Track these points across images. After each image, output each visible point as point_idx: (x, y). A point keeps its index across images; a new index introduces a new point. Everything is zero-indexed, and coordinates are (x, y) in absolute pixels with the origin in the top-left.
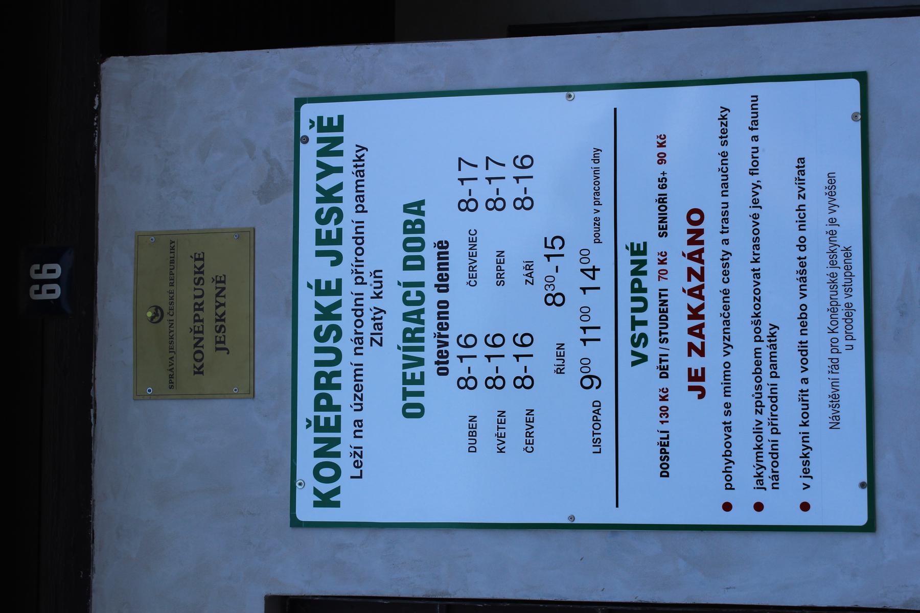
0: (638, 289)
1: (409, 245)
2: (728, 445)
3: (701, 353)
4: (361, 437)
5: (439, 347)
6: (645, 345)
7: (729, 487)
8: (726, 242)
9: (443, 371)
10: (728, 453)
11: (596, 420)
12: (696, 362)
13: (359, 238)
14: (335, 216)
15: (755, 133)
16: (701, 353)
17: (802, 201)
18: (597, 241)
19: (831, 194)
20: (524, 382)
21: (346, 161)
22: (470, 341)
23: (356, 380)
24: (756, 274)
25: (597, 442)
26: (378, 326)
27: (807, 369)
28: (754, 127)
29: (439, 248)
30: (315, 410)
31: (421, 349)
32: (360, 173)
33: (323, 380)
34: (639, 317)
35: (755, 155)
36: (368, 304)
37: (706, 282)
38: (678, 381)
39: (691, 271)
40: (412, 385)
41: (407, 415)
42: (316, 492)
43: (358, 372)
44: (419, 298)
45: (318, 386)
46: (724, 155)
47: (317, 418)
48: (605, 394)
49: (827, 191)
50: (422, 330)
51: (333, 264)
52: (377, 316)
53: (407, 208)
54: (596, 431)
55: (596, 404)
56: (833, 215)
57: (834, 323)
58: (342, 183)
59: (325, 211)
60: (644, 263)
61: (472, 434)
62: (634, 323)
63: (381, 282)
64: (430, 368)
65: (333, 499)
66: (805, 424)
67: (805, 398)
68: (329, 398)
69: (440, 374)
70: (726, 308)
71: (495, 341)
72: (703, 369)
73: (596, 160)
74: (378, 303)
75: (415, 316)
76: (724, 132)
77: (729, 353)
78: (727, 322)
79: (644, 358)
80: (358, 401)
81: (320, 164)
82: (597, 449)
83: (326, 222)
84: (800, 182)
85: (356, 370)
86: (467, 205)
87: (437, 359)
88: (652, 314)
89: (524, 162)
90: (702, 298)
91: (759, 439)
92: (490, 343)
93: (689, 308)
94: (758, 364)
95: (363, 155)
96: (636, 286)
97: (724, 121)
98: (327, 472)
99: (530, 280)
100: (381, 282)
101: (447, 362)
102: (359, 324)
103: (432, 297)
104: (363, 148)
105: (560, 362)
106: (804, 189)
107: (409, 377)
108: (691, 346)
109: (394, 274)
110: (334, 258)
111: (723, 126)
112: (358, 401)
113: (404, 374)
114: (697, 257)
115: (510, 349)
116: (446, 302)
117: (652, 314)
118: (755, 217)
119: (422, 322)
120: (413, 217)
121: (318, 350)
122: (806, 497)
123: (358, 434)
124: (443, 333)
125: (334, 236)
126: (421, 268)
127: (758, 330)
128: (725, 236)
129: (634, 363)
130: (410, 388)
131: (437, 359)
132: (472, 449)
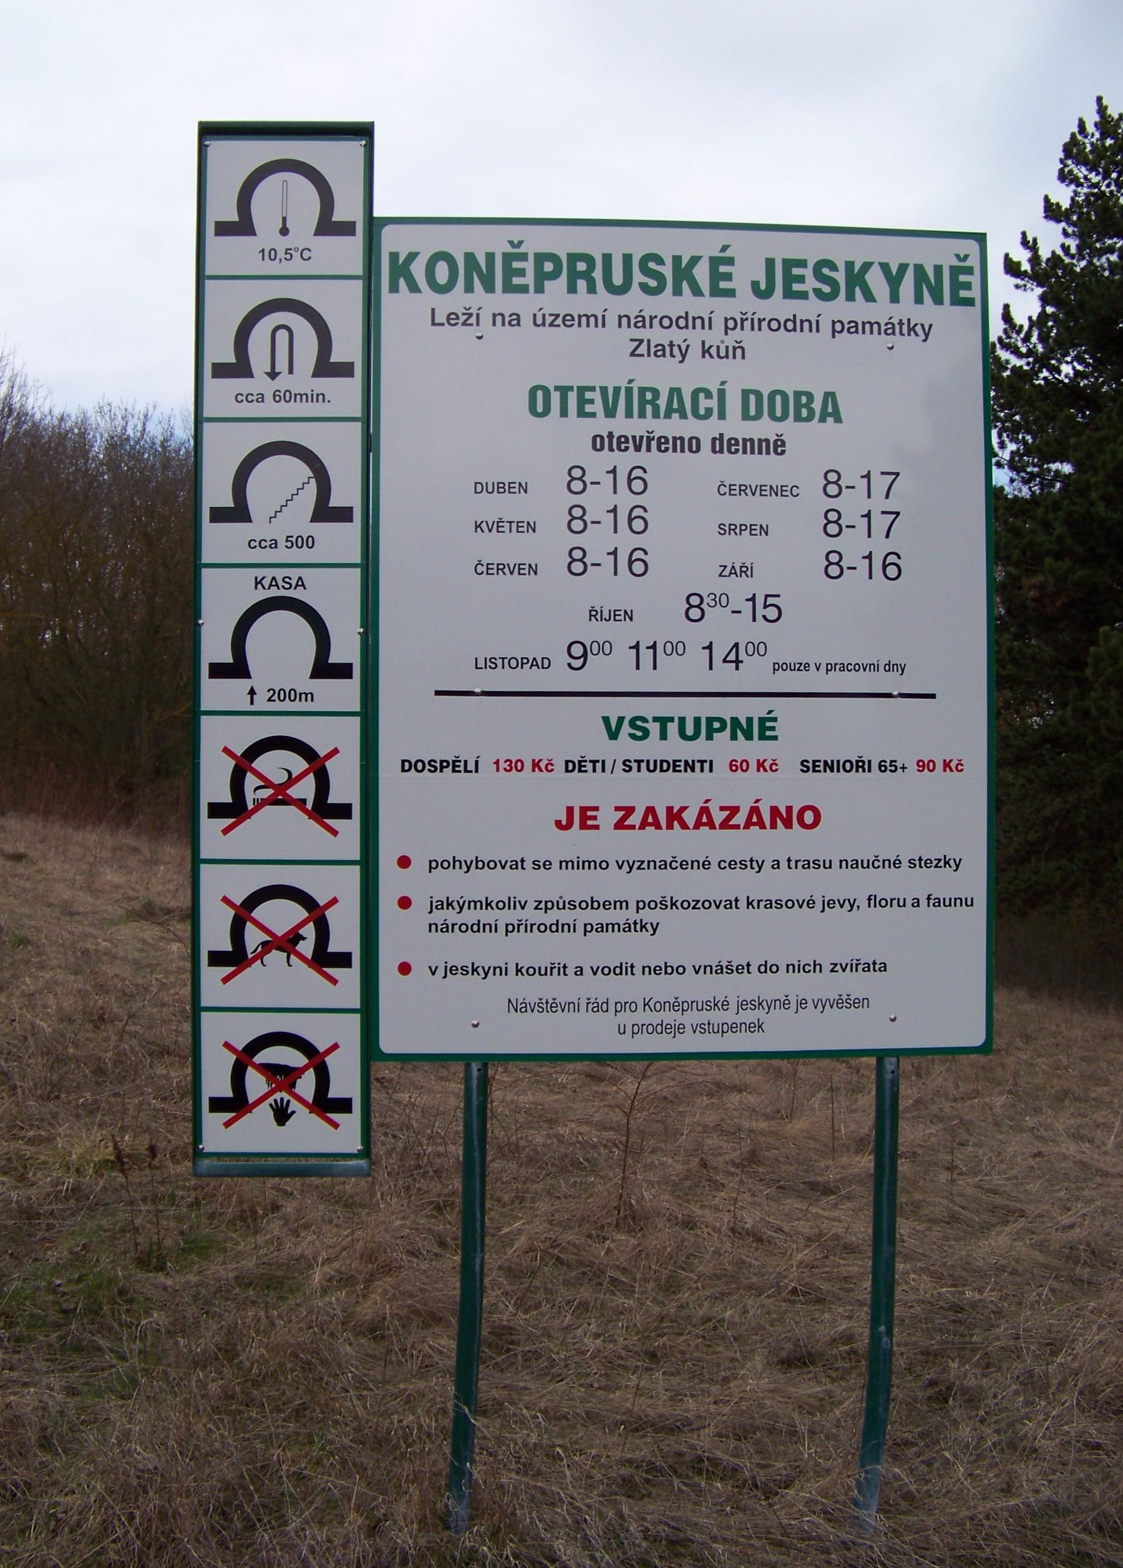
0: (712, 727)
1: (778, 398)
2: (492, 865)
3: (620, 825)
4: (494, 324)
5: (634, 437)
6: (633, 736)
7: (433, 865)
8: (776, 865)
9: (598, 443)
10: (480, 865)
12: (607, 817)
13: (793, 325)
14: (826, 289)
15: (923, 902)
16: (620, 825)
17: (827, 967)
18: (777, 667)
19: (839, 1003)
20: (578, 562)
21: (907, 309)
22: (638, 525)
23: (580, 317)
24: (732, 904)
26: (661, 351)
27: (595, 974)
28: (932, 902)
29: (776, 441)
30: (536, 254)
31: (629, 414)
32: (890, 329)
33: (581, 266)
34: (673, 728)
35: (895, 902)
36: (694, 337)
37: (718, 831)
38: (581, 790)
39: (734, 810)
40: (577, 399)
41: (533, 391)
42: (412, 256)
43: (592, 320)
44: (702, 412)
45: (573, 258)
46: (896, 863)
47: (524, 257)
49: (844, 997)
50: (656, 415)
51: (755, 285)
52: (676, 350)
53: (830, 396)
56: (810, 1004)
57: (658, 1006)
58: (875, 301)
59: (832, 274)
60: (748, 736)
62: (663, 721)
63: (727, 356)
64: (602, 425)
65: (402, 281)
66: (518, 971)
67: (555, 971)
68: (555, 275)
69: (594, 438)
70: (683, 865)
71: (639, 522)
72: (597, 827)
73: (890, 667)
74: (695, 351)
75: (676, 406)
76: (928, 863)
77: (620, 868)
78: (664, 865)
79: (613, 735)
80: (549, 320)
81: (903, 268)
83: (818, 276)
84: (854, 966)
85: (596, 317)
86: (832, 482)
87: (616, 435)
88: (675, 748)
89: (892, 566)
90: (697, 826)
91: (501, 905)
92: (636, 555)
93: (683, 809)
94: (606, 905)
95: (917, 335)
96: (716, 725)
97: (942, 864)
98: (442, 273)
99: (727, 572)
100: (727, 356)
101: (611, 449)
102: (666, 322)
103: (706, 430)
104: (927, 335)
105: (606, 615)
106: (844, 970)
107: (588, 395)
108: (629, 811)
109: (737, 377)
110: (763, 287)
111: (935, 863)
112: (549, 320)
113: (593, 389)
114: (755, 818)
115: (626, 542)
116: (698, 450)
117: (675, 748)
118: (811, 903)
119: (668, 416)
120: (817, 406)
121: (627, 259)
122: (419, 970)
123: (499, 319)
124: (654, 444)
125: (796, 287)
126: (746, 416)
127: (653, 905)
128: (784, 864)
129: (606, 720)
130: (572, 397)
131: (616, 435)
132: (480, 488)
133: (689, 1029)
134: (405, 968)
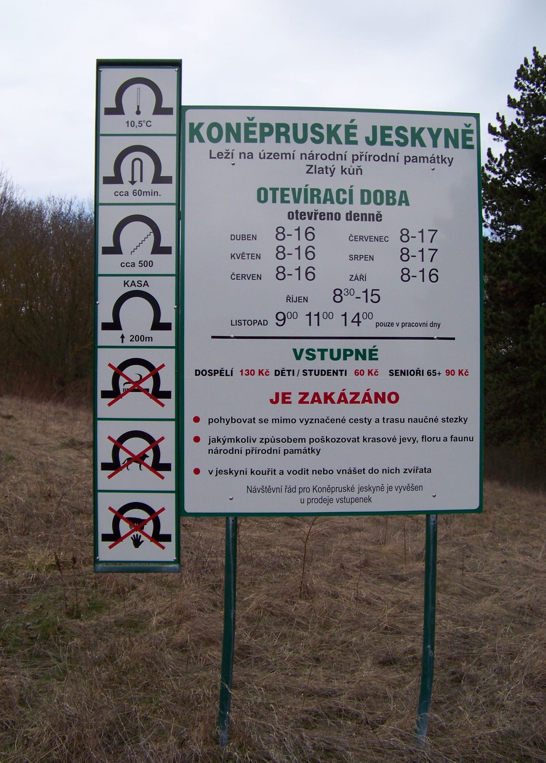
0: (346, 354)
1: (378, 194)
2: (239, 421)
3: (301, 401)
4: (240, 158)
5: (308, 213)
6: (308, 358)
7: (210, 421)
8: (377, 421)
9: (291, 216)
10: (233, 421)
11: (254, 322)
12: (295, 398)
13: (386, 158)
14: (402, 141)
15: (449, 439)
16: (301, 401)
17: (402, 471)
18: (378, 325)
19: (408, 488)
20: (281, 274)
21: (441, 150)
23: (282, 154)
24: (356, 440)
25: (239, 323)
26: (321, 171)
27: (289, 474)
28: (453, 439)
29: (377, 215)
30: (260, 124)
31: (306, 202)
32: (433, 160)
33: (283, 130)
34: (327, 354)
35: (435, 439)
36: (338, 164)
37: (349, 405)
38: (283, 384)
39: (357, 394)
40: (281, 194)
41: (259, 190)
42: (200, 125)
43: (288, 155)
44: (341, 200)
45: (279, 126)
46: (436, 420)
47: (255, 125)
48: (272, 330)
49: (411, 485)
50: (319, 202)
51: (367, 139)
52: (329, 171)
53: (403, 193)
54: (246, 322)
55: (265, 322)
56: (394, 489)
57: (320, 490)
58: (425, 146)
59: (405, 133)
60: (364, 358)
61: (244, 237)
62: (323, 351)
63: (353, 173)
64: (293, 207)
65: (195, 137)
66: (252, 472)
67: (270, 472)
68: (270, 134)
69: (289, 213)
70: (332, 421)
71: (311, 254)
72: (290, 403)
73: (432, 325)
74: (338, 171)
75: (329, 197)
76: (451, 420)
77: (302, 422)
78: (323, 421)
79: (298, 358)
80: (267, 156)
81: (439, 130)
82: (234, 323)
83: (398, 134)
84: (415, 470)
85: (290, 154)
86: (405, 234)
87: (300, 212)
88: (328, 364)
89: (434, 275)
90: (339, 402)
91: (243, 440)
93: (332, 394)
94: (295, 440)
95: (446, 163)
96: (348, 353)
97: (458, 420)
98: (215, 133)
99: (353, 278)
100: (353, 173)
101: (297, 219)
102: (324, 157)
103: (343, 209)
104: (451, 163)
105: (295, 299)
106: (410, 472)
107: (286, 192)
108: (306, 394)
109: (358, 183)
110: (371, 139)
111: (454, 420)
112: (267, 156)
113: (288, 189)
114: (367, 398)
115: (304, 264)
116: (339, 219)
117: (328, 364)
118: (394, 440)
119: (325, 202)
120: (397, 197)
121: (305, 126)
122: (204, 472)
123: (243, 155)
124: (318, 216)
125: (387, 140)
126: (363, 202)
127: (317, 440)
128: (381, 420)
129: (295, 350)
130: (278, 193)
131: (300, 212)
132: (233, 237)
133: (335, 501)
134: (197, 471)
